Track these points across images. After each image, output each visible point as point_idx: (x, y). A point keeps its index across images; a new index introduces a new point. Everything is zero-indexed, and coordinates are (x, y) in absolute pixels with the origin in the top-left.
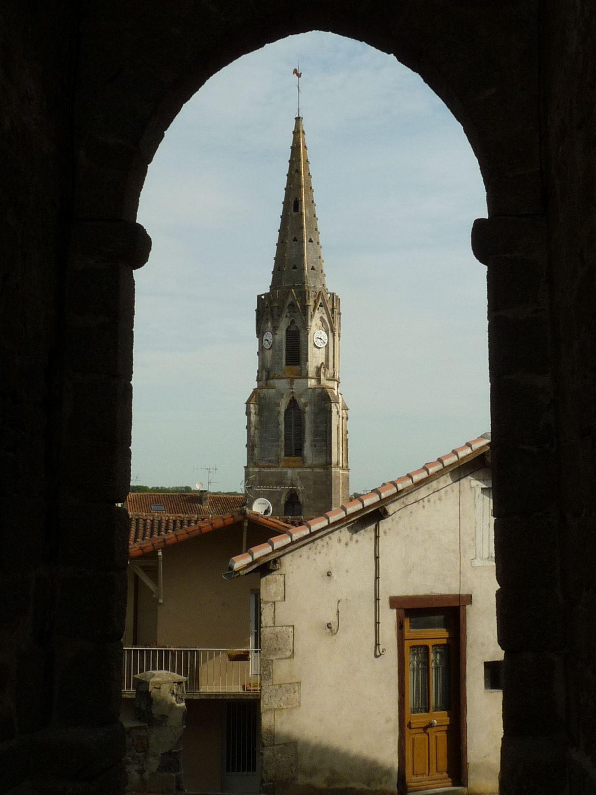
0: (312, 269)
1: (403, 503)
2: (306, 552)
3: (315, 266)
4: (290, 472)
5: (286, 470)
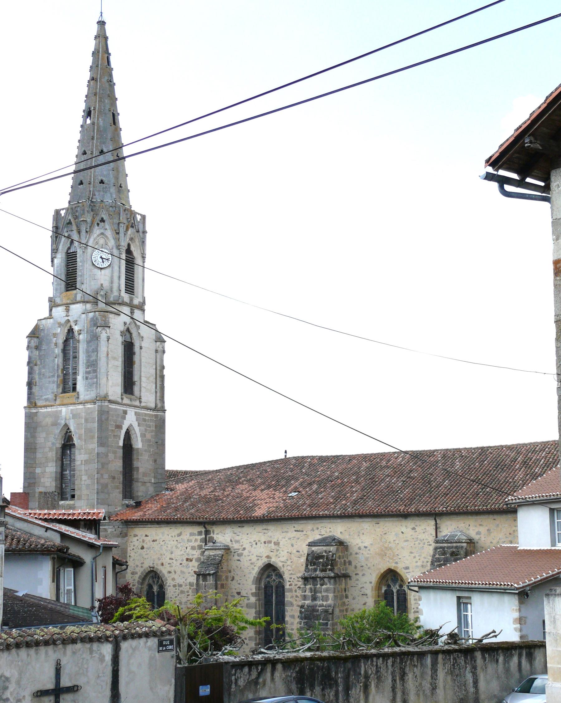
0: (100, 183)
1: (114, 358)
2: (353, 610)
3: (104, 179)
4: (64, 409)
5: (60, 409)
